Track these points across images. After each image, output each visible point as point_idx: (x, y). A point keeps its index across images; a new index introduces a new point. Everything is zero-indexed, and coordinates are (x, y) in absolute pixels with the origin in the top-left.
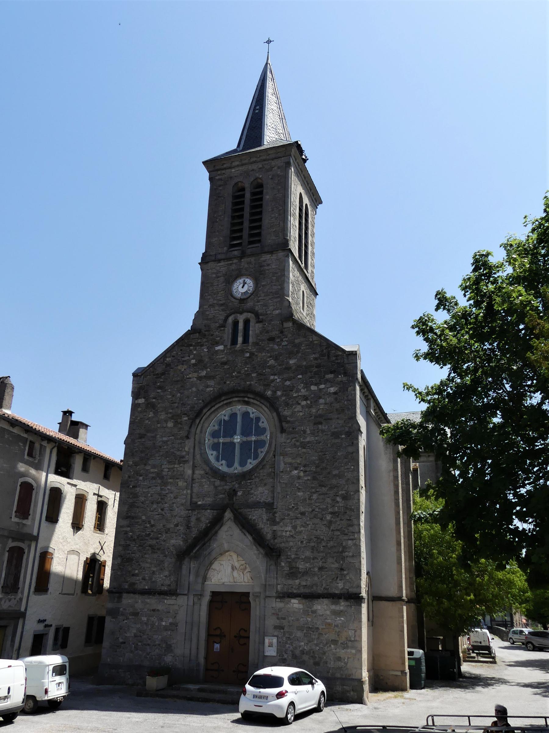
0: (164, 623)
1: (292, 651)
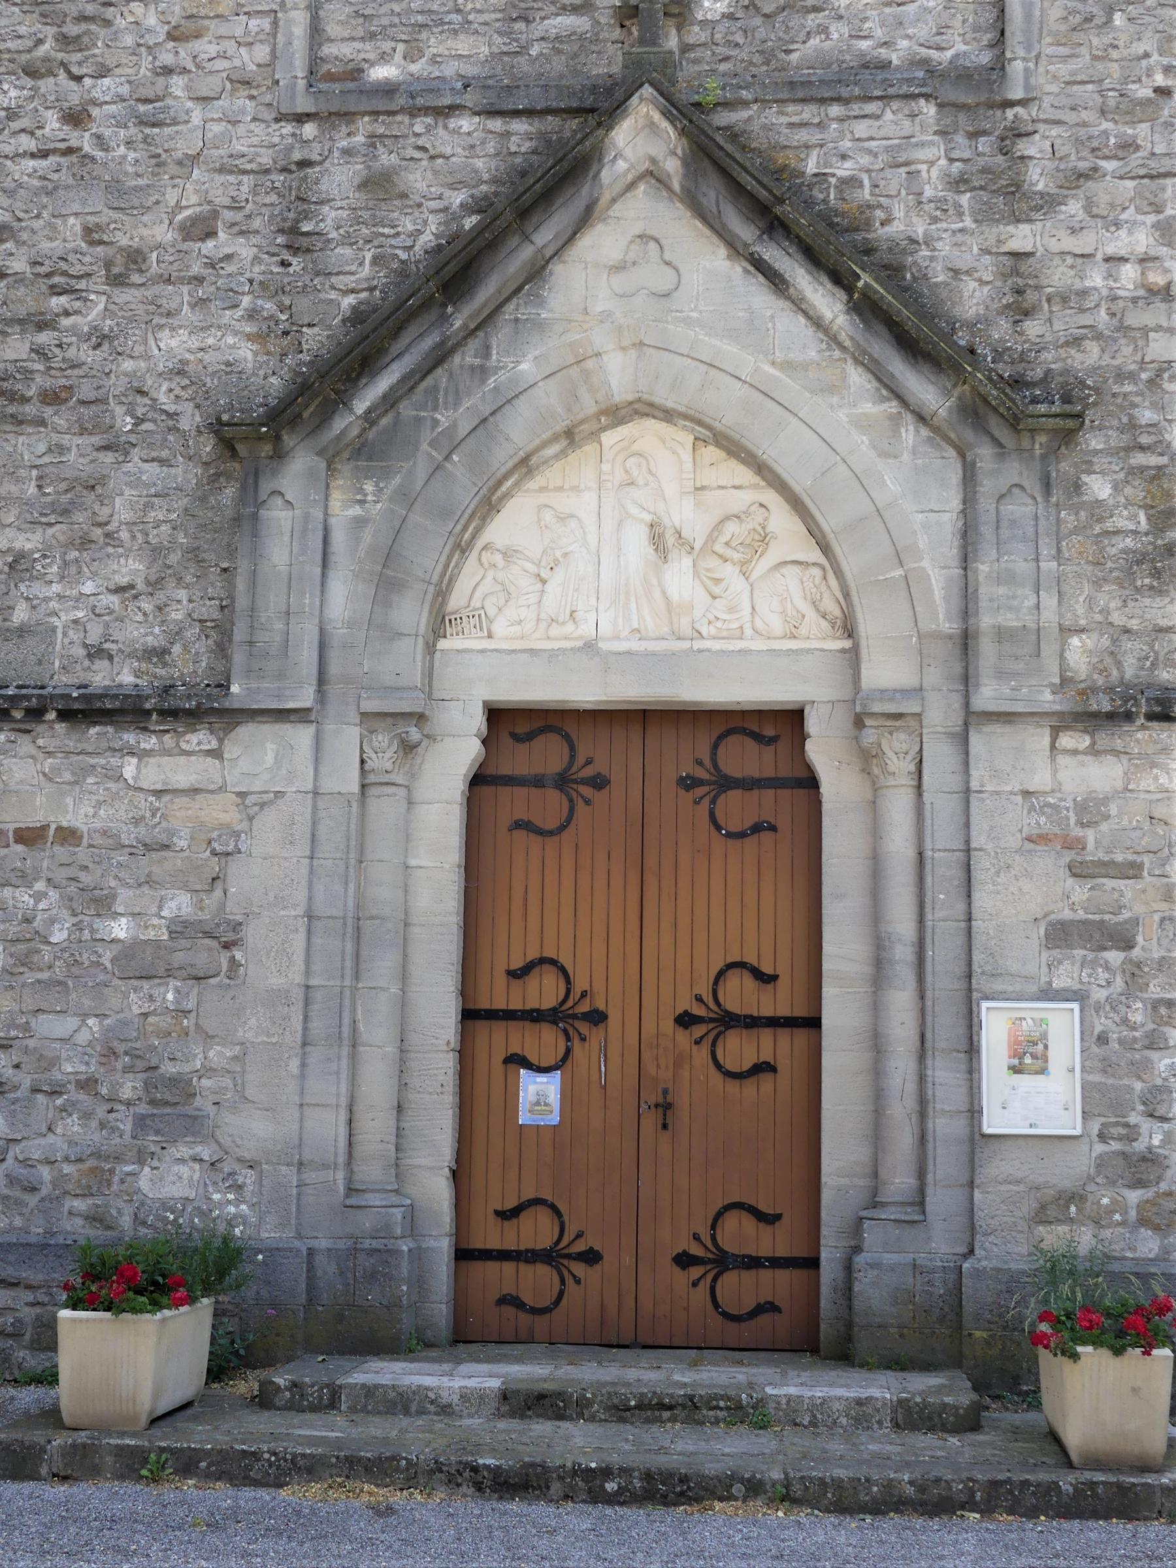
0: (120, 929)
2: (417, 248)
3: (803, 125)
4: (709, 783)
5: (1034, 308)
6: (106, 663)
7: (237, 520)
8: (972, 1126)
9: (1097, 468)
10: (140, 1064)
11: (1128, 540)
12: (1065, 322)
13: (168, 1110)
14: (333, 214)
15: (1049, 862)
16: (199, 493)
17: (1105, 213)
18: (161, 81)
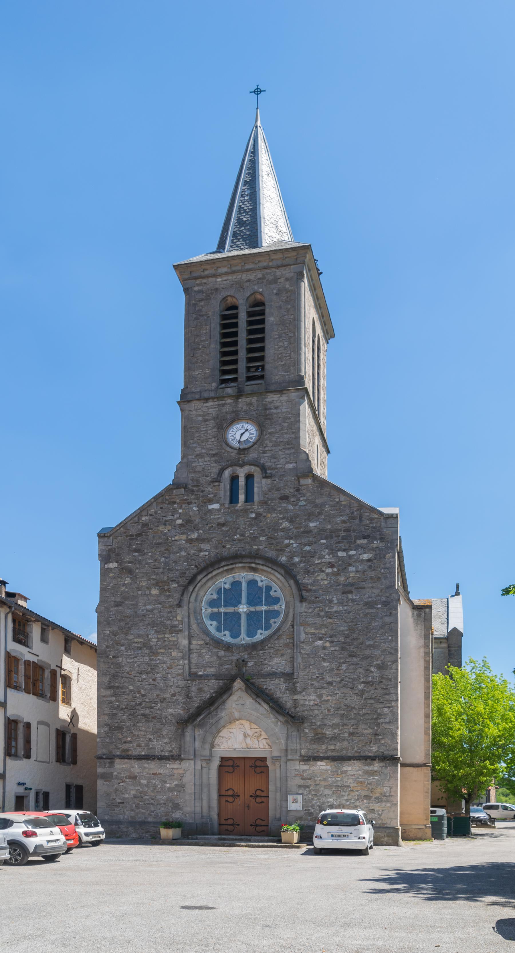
0: (168, 785)
12: (302, 709)
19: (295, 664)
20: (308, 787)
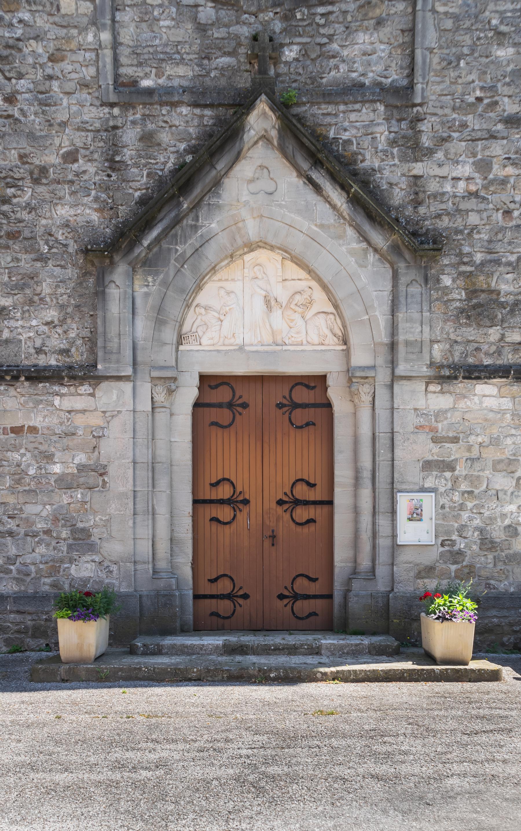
0: (57, 469)
1: (481, 531)
2: (166, 170)
3: (328, 114)
4: (289, 406)
5: (422, 201)
6: (44, 356)
7: (96, 294)
8: (393, 541)
9: (446, 272)
10: (69, 524)
11: (458, 303)
12: (435, 207)
13: (81, 542)
14: (129, 152)
15: (424, 438)
16: (79, 281)
17: (453, 157)
18: (47, 82)
19: (418, 53)
20: (450, 467)
